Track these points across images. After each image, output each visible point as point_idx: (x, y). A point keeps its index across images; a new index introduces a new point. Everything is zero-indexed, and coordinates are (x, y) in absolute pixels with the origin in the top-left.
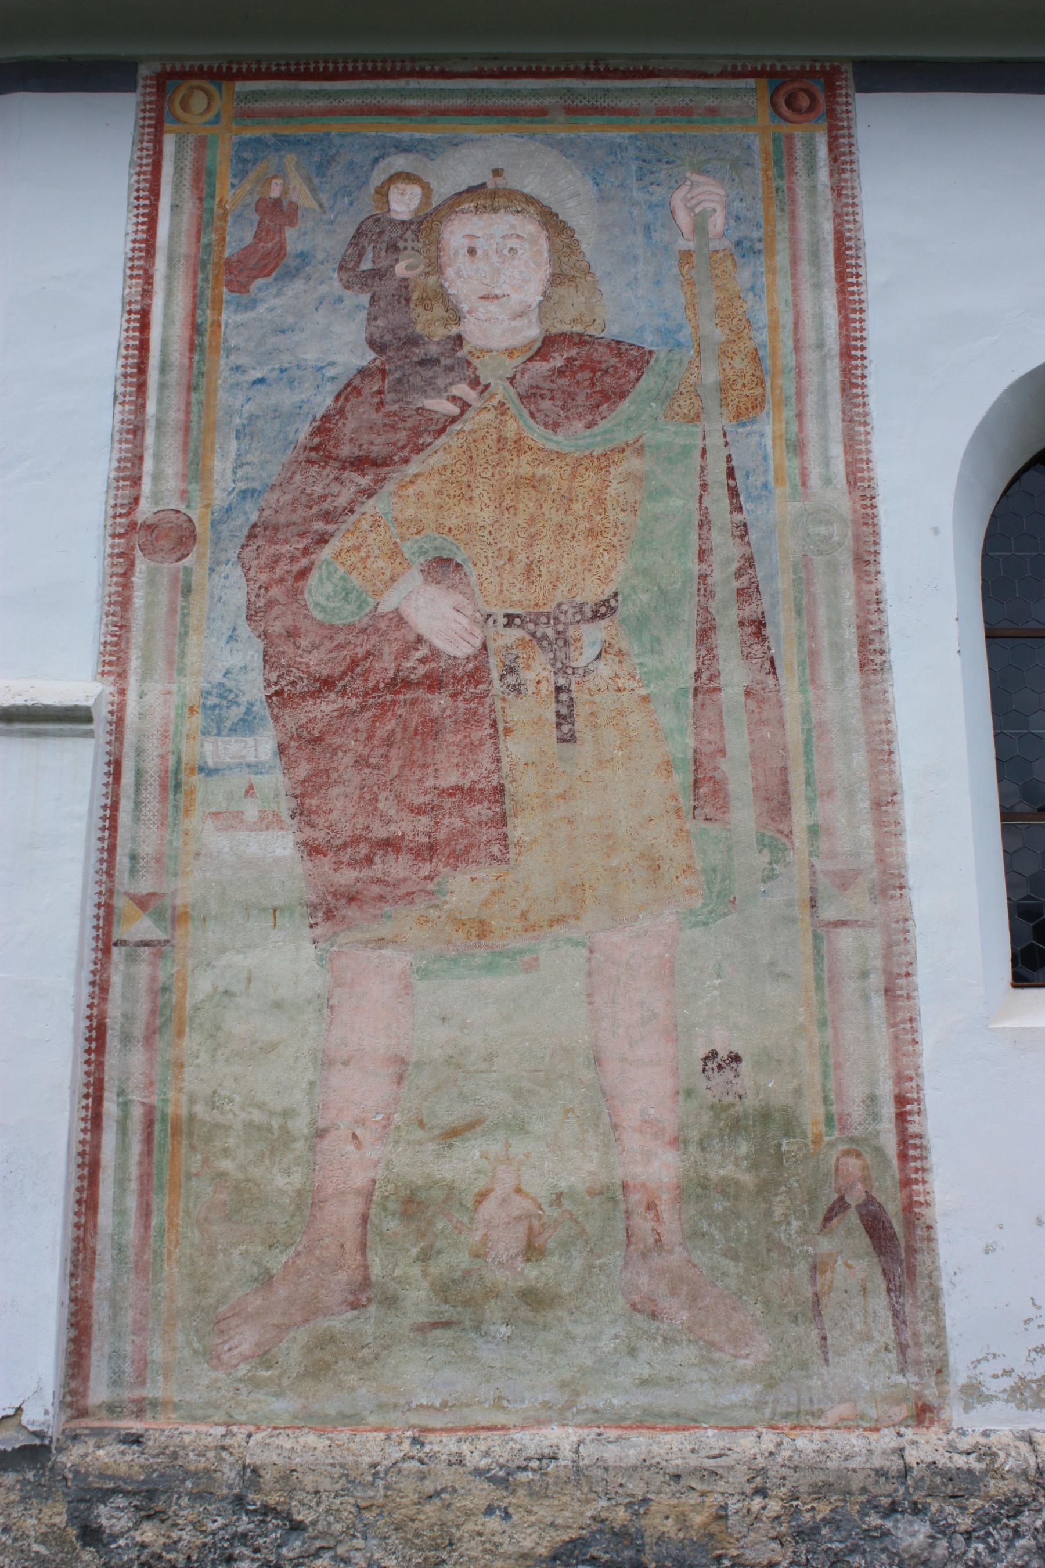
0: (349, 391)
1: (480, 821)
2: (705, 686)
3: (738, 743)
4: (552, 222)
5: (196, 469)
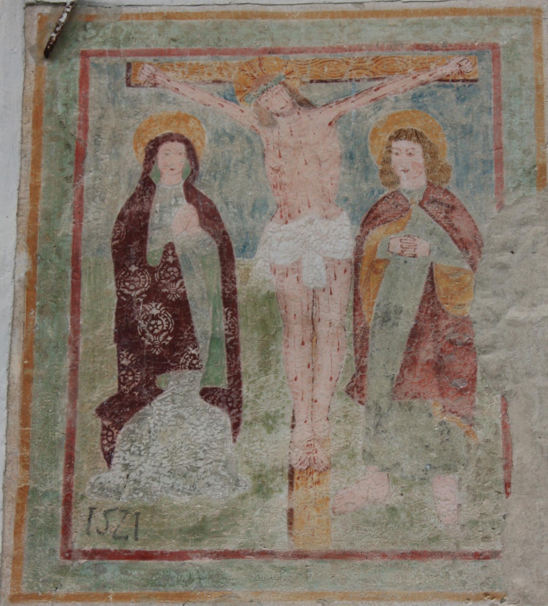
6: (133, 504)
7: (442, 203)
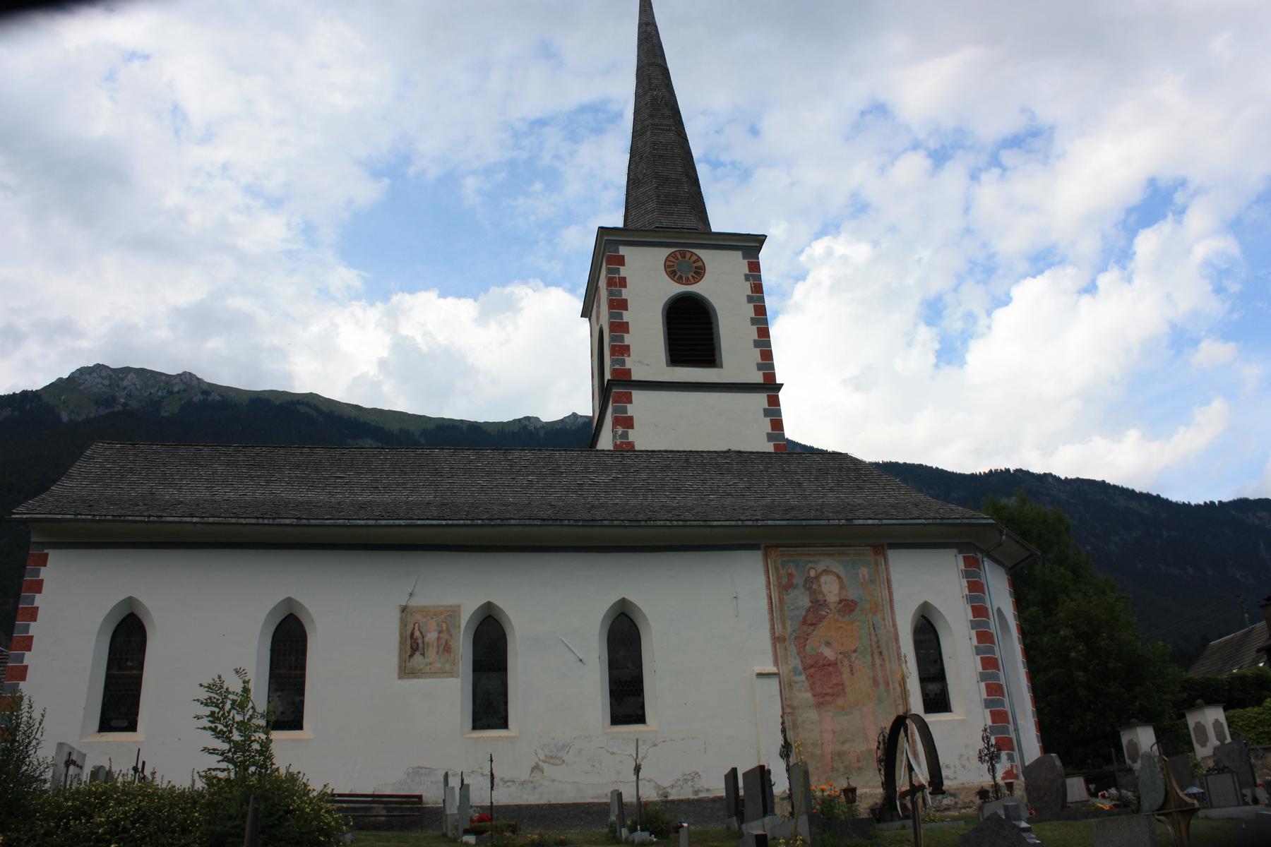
0: (808, 611)
1: (840, 690)
2: (873, 664)
3: (880, 675)
4: (839, 577)
5: (784, 627)
6: (829, 253)
7: (448, 631)
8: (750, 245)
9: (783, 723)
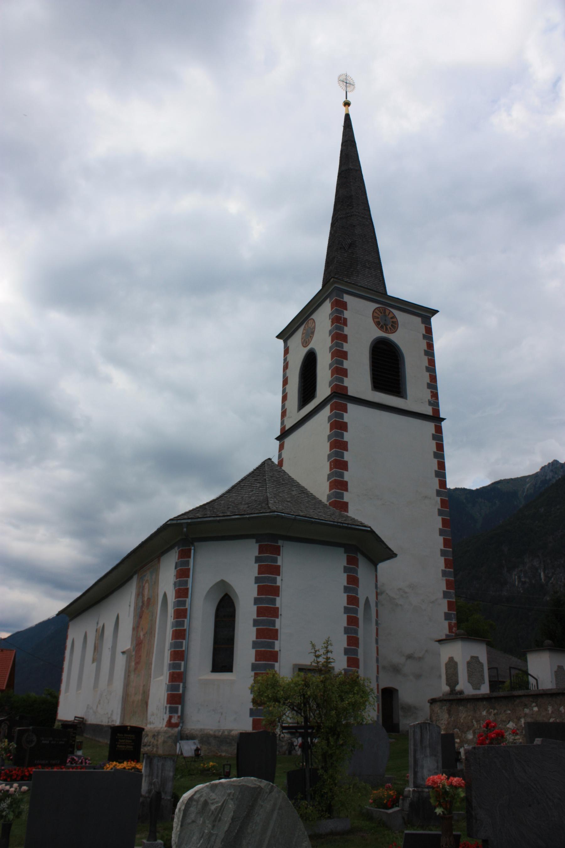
8: (425, 314)
9: (95, 644)
